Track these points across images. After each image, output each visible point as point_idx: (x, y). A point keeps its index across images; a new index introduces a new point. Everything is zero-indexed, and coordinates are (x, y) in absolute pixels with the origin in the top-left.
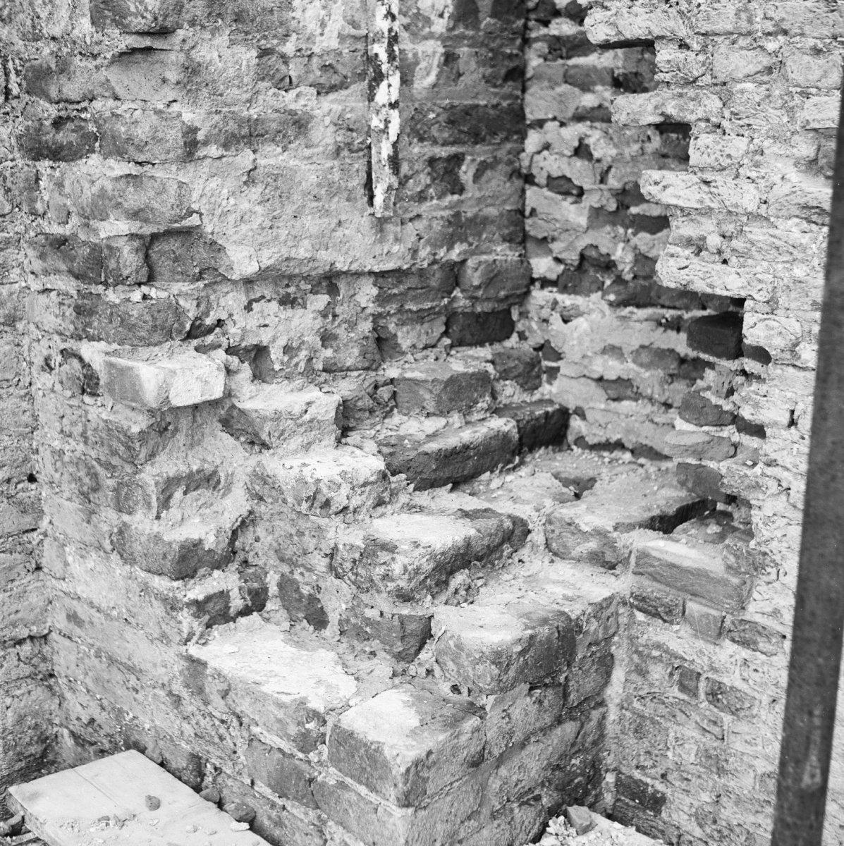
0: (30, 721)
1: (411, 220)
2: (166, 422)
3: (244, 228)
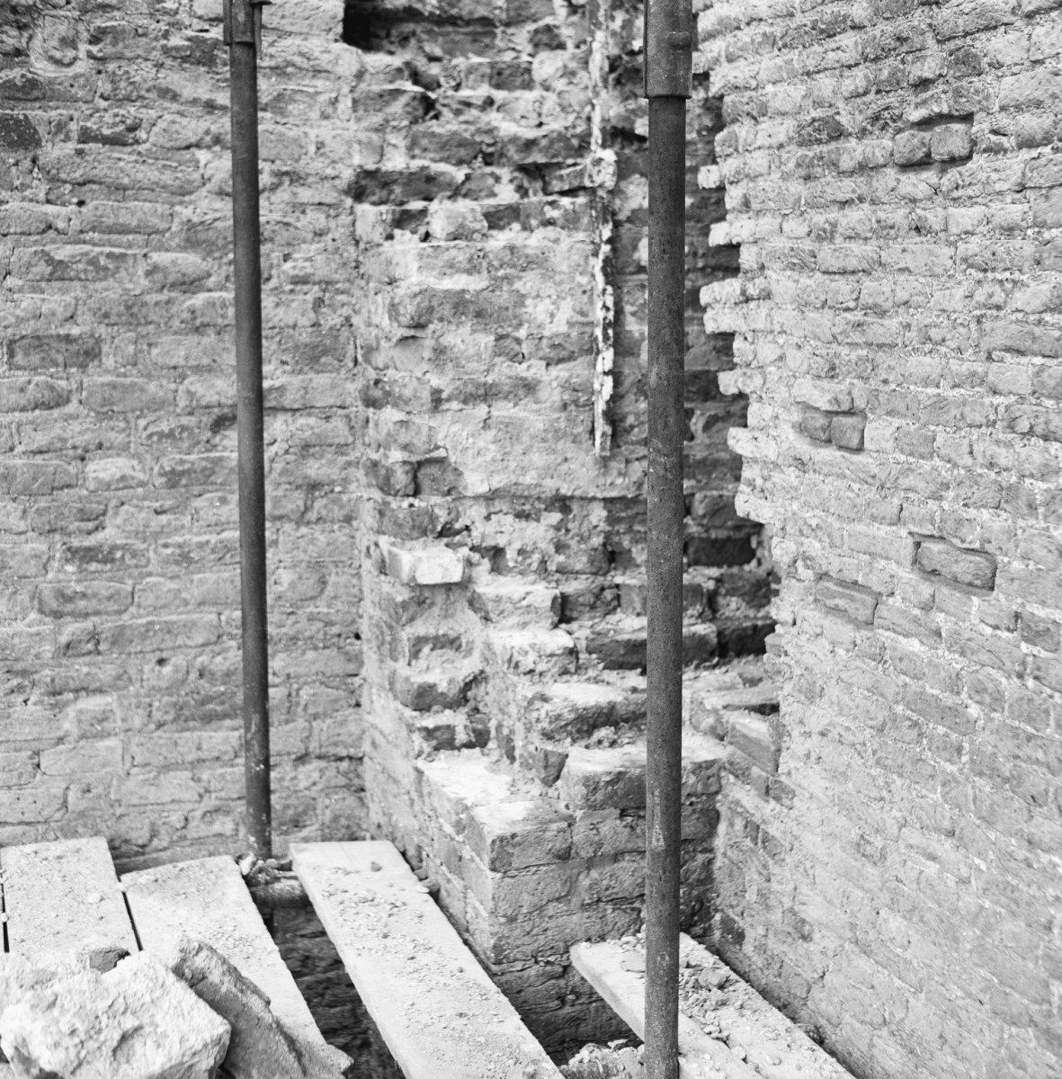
0: (343, 821)
1: (637, 459)
2: (423, 596)
3: (480, 460)
